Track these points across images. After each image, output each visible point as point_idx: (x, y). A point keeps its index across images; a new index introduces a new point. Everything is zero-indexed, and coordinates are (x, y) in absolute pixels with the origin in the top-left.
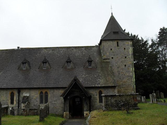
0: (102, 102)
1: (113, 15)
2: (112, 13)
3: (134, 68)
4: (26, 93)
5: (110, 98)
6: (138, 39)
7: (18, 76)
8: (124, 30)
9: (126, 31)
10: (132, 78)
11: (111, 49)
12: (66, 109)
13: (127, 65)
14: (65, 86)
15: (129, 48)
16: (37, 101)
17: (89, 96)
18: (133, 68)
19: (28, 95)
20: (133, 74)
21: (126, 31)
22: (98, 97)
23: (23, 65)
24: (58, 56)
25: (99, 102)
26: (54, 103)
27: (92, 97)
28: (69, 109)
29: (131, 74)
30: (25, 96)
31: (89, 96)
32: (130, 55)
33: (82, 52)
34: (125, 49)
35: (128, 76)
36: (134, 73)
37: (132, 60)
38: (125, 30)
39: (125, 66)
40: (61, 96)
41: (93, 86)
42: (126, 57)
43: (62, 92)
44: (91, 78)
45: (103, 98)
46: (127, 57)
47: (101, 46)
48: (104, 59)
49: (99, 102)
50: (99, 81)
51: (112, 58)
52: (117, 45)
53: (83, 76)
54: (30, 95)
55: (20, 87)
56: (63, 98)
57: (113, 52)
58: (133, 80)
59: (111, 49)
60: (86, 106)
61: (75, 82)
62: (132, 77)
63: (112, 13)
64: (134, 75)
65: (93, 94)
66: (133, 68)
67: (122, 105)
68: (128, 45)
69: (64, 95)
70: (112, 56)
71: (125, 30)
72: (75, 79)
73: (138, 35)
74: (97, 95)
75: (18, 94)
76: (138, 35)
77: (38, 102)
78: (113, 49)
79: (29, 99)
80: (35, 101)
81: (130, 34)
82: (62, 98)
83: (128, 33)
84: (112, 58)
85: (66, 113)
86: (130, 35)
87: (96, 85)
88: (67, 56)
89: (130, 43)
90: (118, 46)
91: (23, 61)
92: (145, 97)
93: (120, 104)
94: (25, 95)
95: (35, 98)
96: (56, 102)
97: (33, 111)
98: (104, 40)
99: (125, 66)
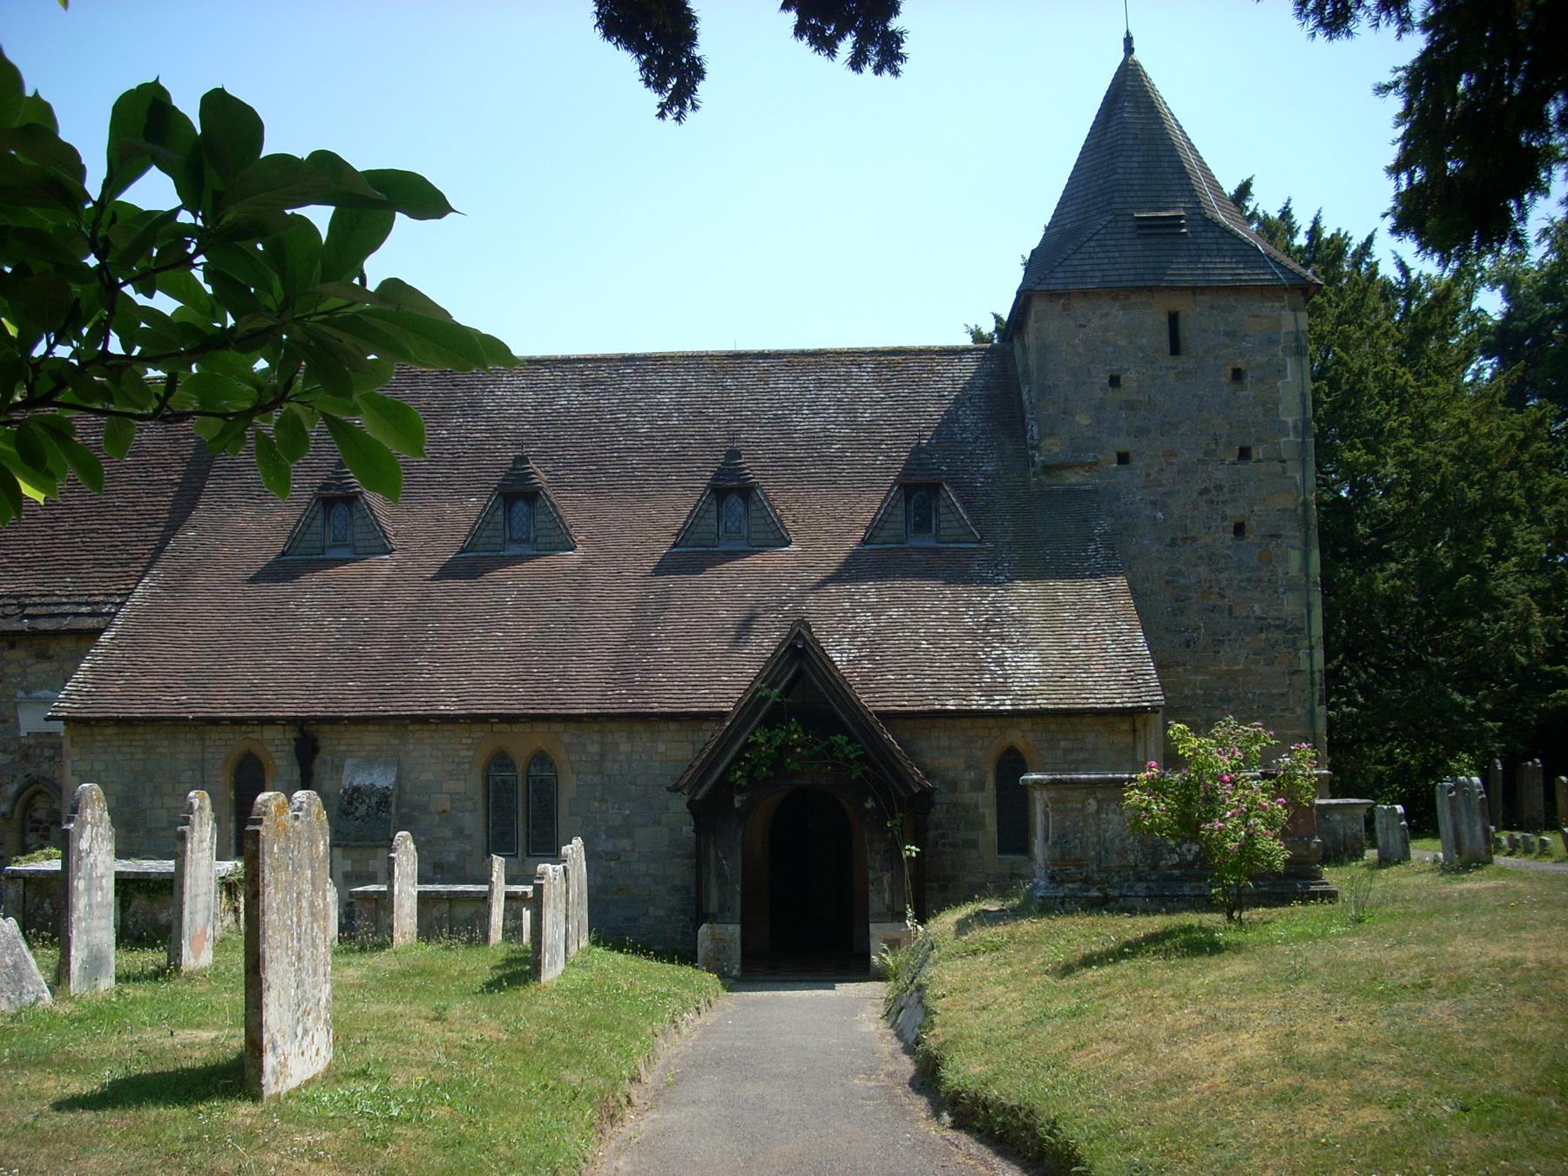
0: (1024, 848)
1: (1138, 56)
2: (1128, 41)
3: (1025, 397)
4: (369, 763)
5: (1092, 805)
6: (1373, 268)
7: (295, 618)
8: (1230, 188)
9: (1265, 202)
10: (1294, 644)
11: (1114, 381)
12: (714, 894)
13: (1252, 523)
14: (703, 707)
15: (1281, 372)
16: (460, 833)
17: (916, 790)
18: (1306, 557)
19: (382, 779)
20: (1309, 606)
21: (1265, 202)
22: (986, 803)
23: (327, 517)
24: (632, 433)
25: (1002, 850)
26: (609, 846)
27: (937, 798)
28: (738, 899)
29: (1291, 606)
30: (357, 789)
31: (916, 790)
32: (1282, 430)
33: (852, 402)
34: (1237, 375)
35: (1262, 625)
36: (1317, 598)
37: (1298, 477)
38: (1244, 190)
39: (1239, 529)
40: (676, 789)
41: (951, 705)
42: (1244, 454)
43: (675, 752)
44: (934, 640)
45: (1039, 801)
46: (1258, 452)
47: (1025, 349)
48: (1048, 469)
49: (1002, 850)
50: (1000, 661)
51: (1123, 459)
52: (1164, 338)
53: (861, 619)
54: (399, 778)
55: (319, 711)
56: (690, 805)
57: (1130, 406)
58: (1302, 654)
59: (1114, 381)
60: (887, 878)
61: (799, 674)
62: (1294, 631)
63: (1128, 41)
64: (1317, 613)
65: (951, 774)
66: (1306, 557)
67: (1191, 865)
68: (1272, 342)
69: (700, 784)
70: (1125, 443)
71: (1244, 190)
72: (792, 646)
73: (1370, 239)
74: (979, 786)
75: (297, 770)
76: (1370, 239)
77: (470, 836)
78: (1130, 380)
79: (393, 810)
80: (448, 833)
81: (1303, 221)
82: (679, 804)
83: (1286, 213)
84: (1123, 459)
85: (720, 929)
86: (1301, 240)
87: (978, 702)
88: (719, 436)
89: (1292, 320)
90: (1175, 349)
91: (325, 487)
92: (1399, 808)
93: (1172, 851)
94: (361, 780)
95: (441, 802)
96: (625, 844)
97: (445, 907)
98: (1053, 295)
99: (1239, 529)
